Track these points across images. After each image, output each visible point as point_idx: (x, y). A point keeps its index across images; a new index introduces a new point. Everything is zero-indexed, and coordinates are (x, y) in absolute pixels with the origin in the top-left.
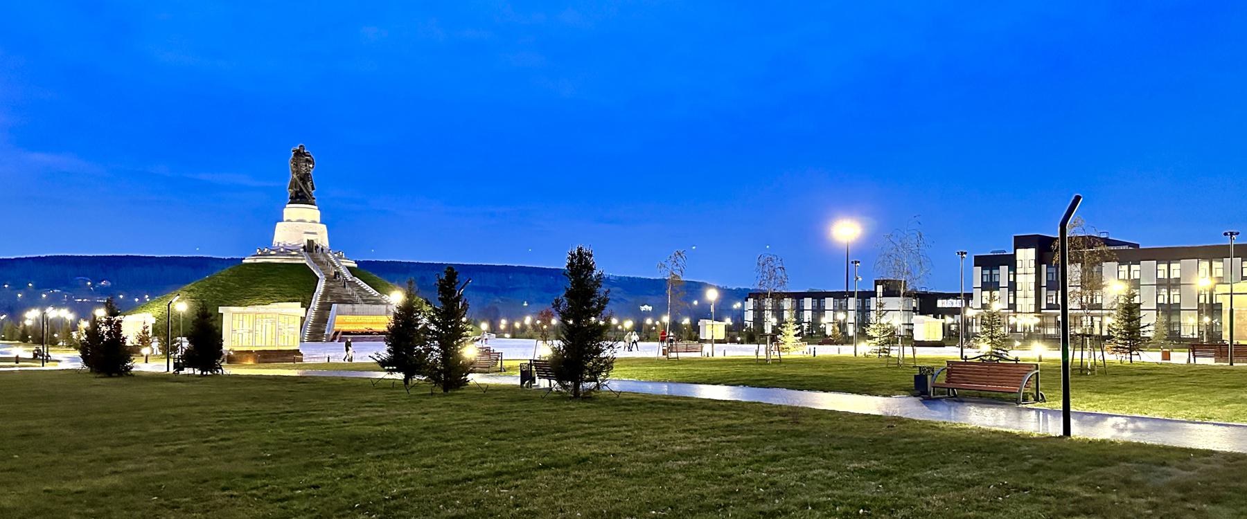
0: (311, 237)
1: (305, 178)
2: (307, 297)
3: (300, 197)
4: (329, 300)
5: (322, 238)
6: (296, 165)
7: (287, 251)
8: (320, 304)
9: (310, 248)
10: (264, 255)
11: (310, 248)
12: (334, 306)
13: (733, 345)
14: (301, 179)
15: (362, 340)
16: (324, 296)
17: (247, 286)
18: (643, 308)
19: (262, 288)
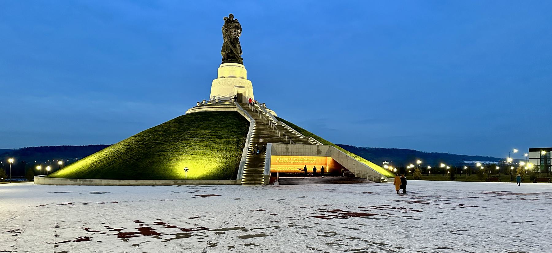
0: (241, 91)
1: (234, 42)
2: (241, 138)
3: (232, 56)
4: (261, 141)
5: (249, 93)
6: (227, 31)
7: (221, 102)
8: (254, 144)
9: (239, 98)
10: (202, 105)
11: (239, 98)
12: (269, 146)
13: (235, 186)
14: (231, 43)
15: (294, 184)
16: (257, 136)
17: (186, 130)
18: (408, 167)
19: (198, 131)
